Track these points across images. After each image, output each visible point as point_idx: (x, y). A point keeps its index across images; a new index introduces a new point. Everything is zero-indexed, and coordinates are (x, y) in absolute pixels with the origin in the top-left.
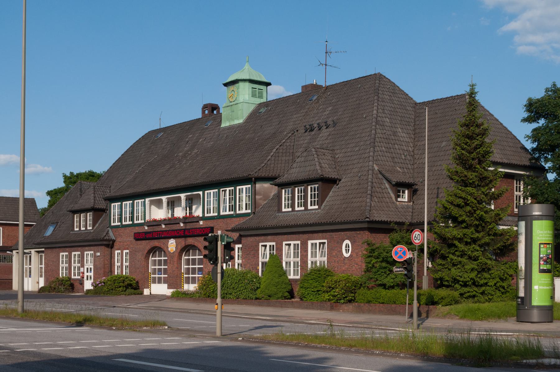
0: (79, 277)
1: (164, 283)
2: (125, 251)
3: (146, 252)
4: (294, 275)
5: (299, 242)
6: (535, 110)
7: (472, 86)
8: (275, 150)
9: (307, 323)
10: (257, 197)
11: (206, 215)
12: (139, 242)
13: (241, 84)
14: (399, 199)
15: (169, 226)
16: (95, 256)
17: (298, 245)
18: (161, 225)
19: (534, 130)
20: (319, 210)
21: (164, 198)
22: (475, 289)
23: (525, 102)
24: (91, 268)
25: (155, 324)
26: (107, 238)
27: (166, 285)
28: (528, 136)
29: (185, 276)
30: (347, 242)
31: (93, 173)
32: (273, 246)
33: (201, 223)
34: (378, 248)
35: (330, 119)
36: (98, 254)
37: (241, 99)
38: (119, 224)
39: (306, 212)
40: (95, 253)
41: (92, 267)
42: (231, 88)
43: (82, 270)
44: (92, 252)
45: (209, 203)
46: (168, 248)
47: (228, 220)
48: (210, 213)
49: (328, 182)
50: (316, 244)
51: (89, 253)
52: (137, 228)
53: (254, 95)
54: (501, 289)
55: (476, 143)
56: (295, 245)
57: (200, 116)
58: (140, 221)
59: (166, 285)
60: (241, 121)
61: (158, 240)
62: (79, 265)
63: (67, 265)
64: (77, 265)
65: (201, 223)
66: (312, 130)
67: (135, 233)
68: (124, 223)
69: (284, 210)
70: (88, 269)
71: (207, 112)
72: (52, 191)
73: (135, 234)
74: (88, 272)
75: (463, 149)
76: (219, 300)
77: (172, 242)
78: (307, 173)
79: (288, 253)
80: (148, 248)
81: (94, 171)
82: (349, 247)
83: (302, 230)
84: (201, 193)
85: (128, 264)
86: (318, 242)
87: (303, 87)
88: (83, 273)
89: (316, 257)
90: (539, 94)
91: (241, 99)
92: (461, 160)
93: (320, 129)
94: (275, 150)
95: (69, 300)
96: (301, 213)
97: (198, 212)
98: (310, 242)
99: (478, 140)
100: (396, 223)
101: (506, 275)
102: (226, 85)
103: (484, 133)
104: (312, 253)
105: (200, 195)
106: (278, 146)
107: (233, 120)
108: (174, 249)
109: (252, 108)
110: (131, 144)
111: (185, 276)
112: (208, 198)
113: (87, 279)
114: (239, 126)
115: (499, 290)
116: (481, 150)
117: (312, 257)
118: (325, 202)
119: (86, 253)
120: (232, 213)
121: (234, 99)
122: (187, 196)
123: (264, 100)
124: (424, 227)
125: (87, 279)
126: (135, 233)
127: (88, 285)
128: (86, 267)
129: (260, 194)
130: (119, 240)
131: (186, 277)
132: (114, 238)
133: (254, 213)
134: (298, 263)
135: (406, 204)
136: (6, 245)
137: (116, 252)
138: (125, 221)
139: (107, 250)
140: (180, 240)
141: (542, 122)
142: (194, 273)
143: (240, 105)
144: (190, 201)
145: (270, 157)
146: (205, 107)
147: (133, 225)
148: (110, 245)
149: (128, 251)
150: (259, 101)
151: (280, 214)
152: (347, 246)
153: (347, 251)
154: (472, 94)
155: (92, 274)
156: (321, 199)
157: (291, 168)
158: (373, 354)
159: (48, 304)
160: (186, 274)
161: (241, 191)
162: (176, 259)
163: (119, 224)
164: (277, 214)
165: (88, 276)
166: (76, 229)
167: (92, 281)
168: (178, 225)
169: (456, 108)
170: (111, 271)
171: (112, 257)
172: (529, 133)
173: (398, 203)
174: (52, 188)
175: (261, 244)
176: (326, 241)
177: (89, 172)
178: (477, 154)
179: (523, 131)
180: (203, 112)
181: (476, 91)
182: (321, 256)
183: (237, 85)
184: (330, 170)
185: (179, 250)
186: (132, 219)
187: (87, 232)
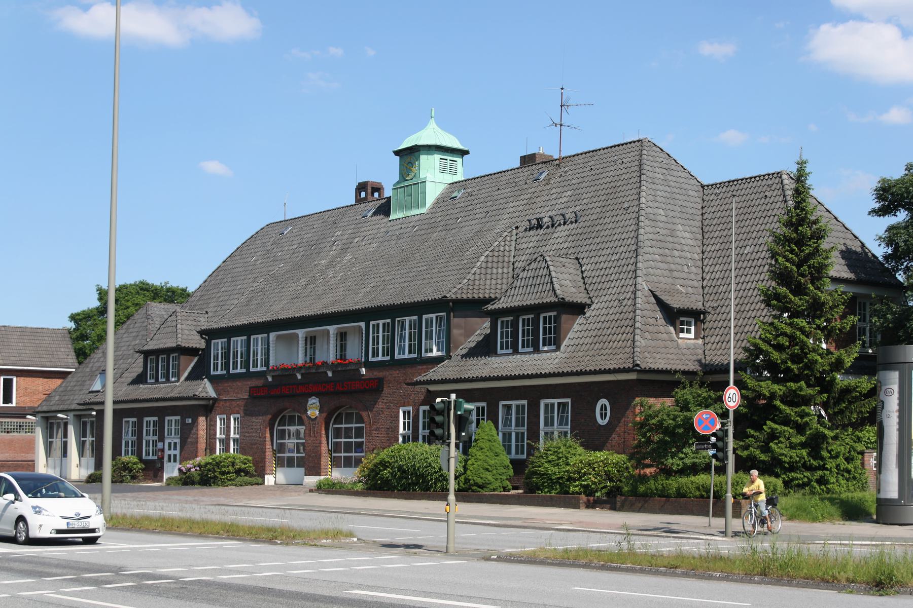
1: (298, 466)
5: (525, 402)
6: (890, 197)
7: (802, 164)
9: (557, 530)
11: (371, 359)
14: (681, 335)
17: (523, 406)
19: (890, 229)
22: (807, 474)
23: (874, 184)
24: (175, 444)
25: (336, 534)
27: (302, 470)
28: (880, 238)
29: (363, 440)
30: (604, 401)
31: (148, 284)
32: (483, 408)
34: (659, 412)
35: (571, 210)
38: (224, 372)
40: (183, 419)
41: (178, 441)
43: (160, 445)
44: (178, 418)
45: (376, 340)
48: (378, 356)
50: (553, 405)
51: (173, 418)
53: (443, 170)
54: (846, 475)
55: (807, 251)
56: (518, 406)
58: (259, 369)
59: (302, 470)
62: (156, 438)
63: (135, 438)
64: (152, 438)
67: (250, 388)
68: (232, 371)
70: (170, 444)
72: (78, 314)
74: (170, 449)
75: (787, 260)
76: (452, 497)
77: (314, 401)
79: (507, 419)
81: (150, 281)
82: (606, 410)
84: (363, 324)
86: (556, 401)
88: (163, 450)
89: (552, 425)
90: (896, 173)
92: (782, 277)
95: (143, 494)
97: (354, 352)
98: (543, 403)
99: (810, 246)
100: (684, 373)
101: (852, 453)
103: (819, 235)
104: (546, 418)
111: (363, 440)
115: (843, 476)
116: (778, 249)
117: (546, 425)
119: (167, 418)
120: (415, 356)
123: (459, 177)
124: (729, 377)
125: (169, 460)
126: (250, 388)
128: (167, 442)
134: (523, 434)
135: (692, 341)
136: (21, 404)
138: (235, 367)
141: (902, 216)
146: (362, 187)
147: (248, 375)
152: (603, 408)
153: (603, 416)
154: (800, 178)
158: (710, 578)
159: (151, 504)
161: (429, 323)
163: (224, 372)
165: (169, 456)
169: (767, 193)
172: (882, 232)
173: (680, 341)
174: (77, 309)
176: (569, 400)
177: (141, 282)
178: (809, 267)
179: (872, 233)
181: (807, 170)
184: (574, 290)
185: (324, 415)
186: (246, 364)
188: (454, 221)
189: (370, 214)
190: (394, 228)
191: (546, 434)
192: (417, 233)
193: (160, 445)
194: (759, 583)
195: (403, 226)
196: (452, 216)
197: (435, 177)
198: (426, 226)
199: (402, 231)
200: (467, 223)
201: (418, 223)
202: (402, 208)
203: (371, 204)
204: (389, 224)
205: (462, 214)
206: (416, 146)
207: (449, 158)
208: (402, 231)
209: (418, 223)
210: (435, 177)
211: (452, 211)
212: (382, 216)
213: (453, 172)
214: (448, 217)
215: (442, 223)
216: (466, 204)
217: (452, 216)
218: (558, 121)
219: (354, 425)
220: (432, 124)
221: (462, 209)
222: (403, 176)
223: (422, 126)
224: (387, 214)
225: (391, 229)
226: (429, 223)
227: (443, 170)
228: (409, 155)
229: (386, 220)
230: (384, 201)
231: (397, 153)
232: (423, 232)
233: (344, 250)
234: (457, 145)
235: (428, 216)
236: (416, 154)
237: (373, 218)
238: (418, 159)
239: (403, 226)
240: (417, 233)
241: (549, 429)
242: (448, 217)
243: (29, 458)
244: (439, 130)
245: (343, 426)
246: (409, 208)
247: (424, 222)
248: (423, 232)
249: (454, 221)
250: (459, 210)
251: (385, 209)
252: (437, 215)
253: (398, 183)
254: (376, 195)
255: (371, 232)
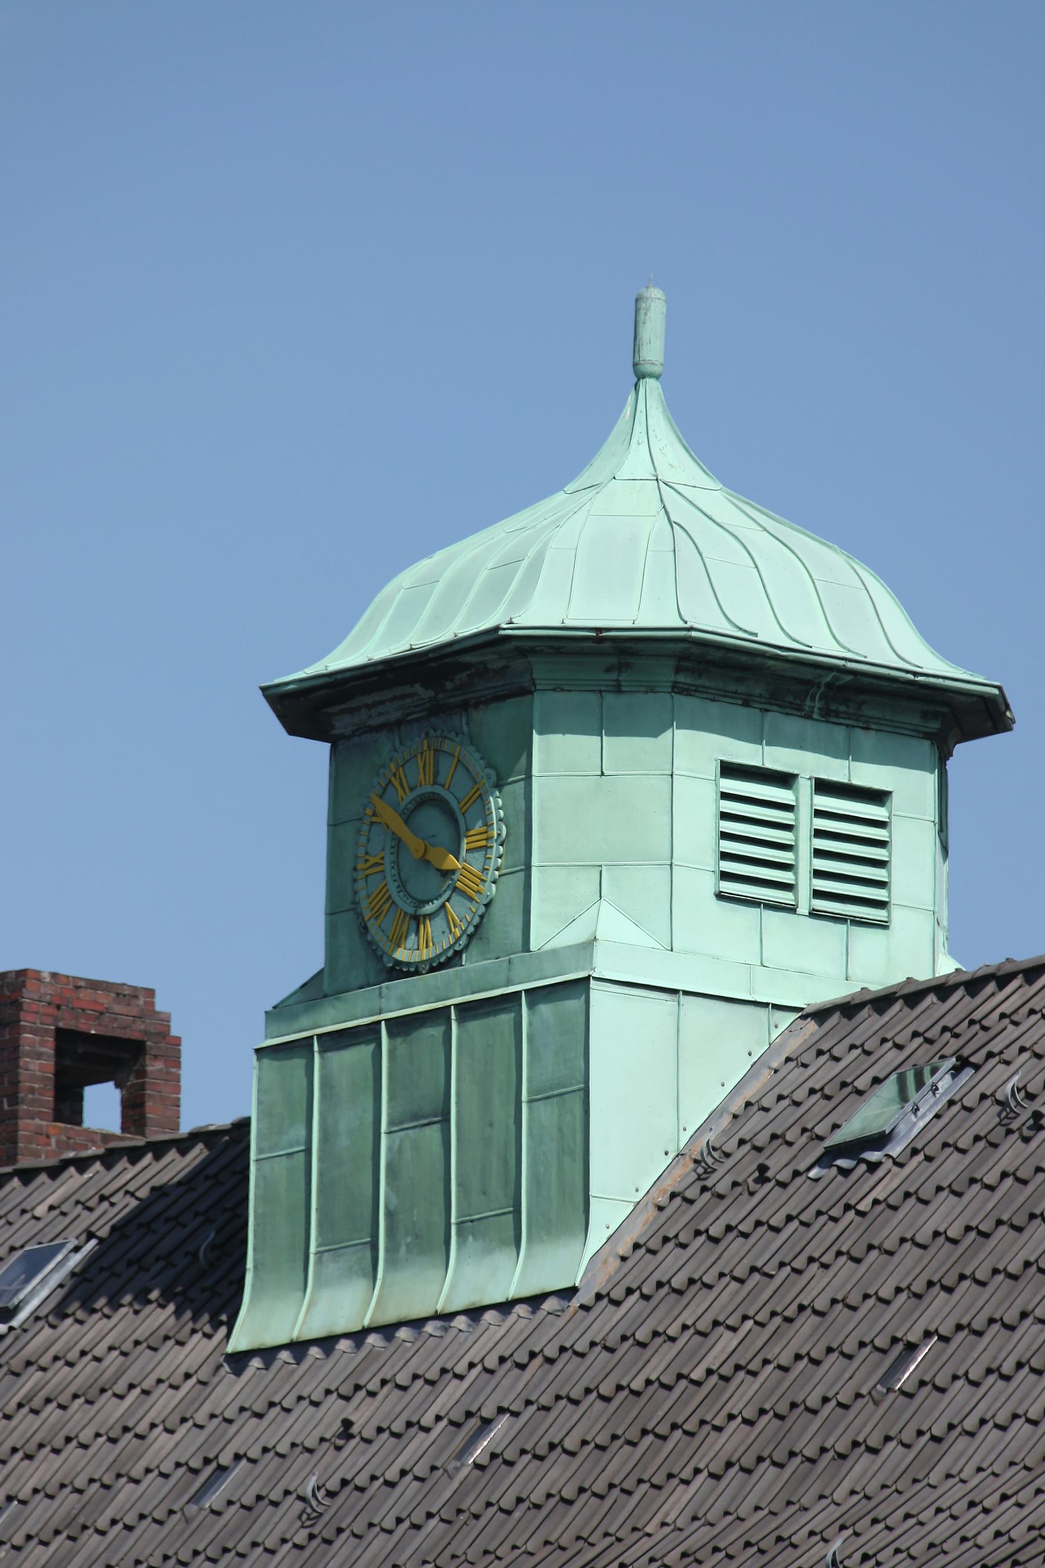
53: (748, 878)
123: (910, 948)
188: (866, 1373)
189: (38, 1293)
190: (279, 1431)
192: (506, 1487)
194: (81, 979)
195: (364, 1414)
196: (846, 1328)
197: (680, 961)
198: (592, 1421)
199: (353, 1461)
200: (996, 1399)
201: (510, 1388)
202: (359, 1240)
203: (50, 1193)
204: (229, 1392)
205: (940, 1312)
206: (492, 641)
207: (809, 764)
208: (353, 1461)
209: (510, 1388)
210: (680, 961)
211: (843, 1277)
212: (159, 1317)
213: (855, 900)
214: (804, 1334)
215: (744, 1395)
216: (978, 1206)
217: (846, 1328)
220: (650, 450)
221: (940, 1262)
222: (365, 931)
223: (559, 453)
224: (212, 1290)
225: (247, 1436)
226: (618, 1377)
227: (748, 878)
228: (424, 742)
229: (199, 1349)
230: (175, 1167)
231: (304, 708)
232: (557, 1475)
234: (887, 638)
235: (607, 1322)
236: (494, 720)
237: (69, 1333)
238: (511, 765)
239: (364, 1414)
240: (506, 1487)
242: (804, 1334)
244: (716, 499)
246: (427, 1241)
247: (573, 1376)
248: (557, 1475)
249: (866, 1373)
250: (906, 1269)
251: (186, 1243)
252: (697, 1309)
253: (314, 992)
254: (102, 1106)
255: (45, 1469)
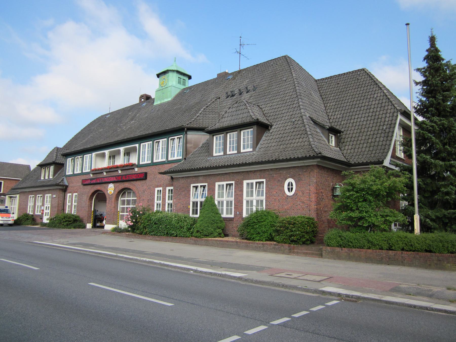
0: (40, 214)
2: (74, 194)
3: (90, 194)
4: (227, 213)
8: (202, 109)
10: (189, 145)
12: (86, 187)
13: (170, 74)
15: (109, 173)
16: (52, 198)
18: (103, 173)
20: (254, 152)
21: (107, 152)
26: (62, 184)
29: (120, 214)
30: (290, 180)
33: (136, 169)
36: (55, 196)
37: (170, 84)
39: (239, 155)
41: (50, 206)
42: (162, 77)
43: (43, 207)
44: (50, 195)
46: (108, 191)
47: (160, 167)
49: (262, 127)
52: (84, 176)
53: (179, 82)
57: (138, 102)
60: (170, 99)
61: (100, 185)
65: (136, 169)
66: (233, 96)
69: (214, 155)
71: (143, 100)
73: (83, 181)
78: (240, 120)
80: (92, 191)
83: (236, 170)
85: (76, 204)
87: (218, 75)
88: (43, 210)
89: (252, 196)
91: (170, 84)
93: (240, 94)
94: (202, 109)
95: (30, 231)
96: (234, 156)
97: (134, 160)
98: (245, 182)
102: (158, 76)
105: (136, 147)
106: (205, 107)
107: (164, 99)
108: (113, 192)
109: (178, 91)
110: (89, 123)
111: (120, 214)
112: (143, 155)
113: (46, 215)
114: (168, 103)
117: (219, 197)
118: (259, 145)
121: (165, 85)
122: (126, 150)
125: (46, 215)
127: (45, 220)
128: (45, 206)
129: (191, 143)
130: (71, 185)
131: (121, 215)
132: (67, 184)
133: (185, 159)
134: (231, 202)
137: (68, 195)
139: (61, 194)
140: (117, 184)
142: (128, 204)
143: (169, 88)
144: (128, 153)
145: (198, 114)
146: (142, 97)
148: (65, 189)
149: (76, 194)
150: (183, 87)
151: (212, 158)
152: (290, 184)
153: (290, 190)
155: (49, 211)
156: (257, 140)
157: (222, 118)
160: (122, 212)
162: (113, 199)
164: (209, 158)
165: (46, 213)
166: (42, 178)
167: (49, 216)
168: (117, 172)
170: (64, 209)
171: (65, 199)
175: (192, 185)
180: (140, 100)
182: (228, 197)
183: (167, 75)
185: (116, 193)
187: (49, 180)
191: (247, 202)
193: (43, 207)
218: (238, 50)
219: (131, 199)
233: (132, 120)
241: (250, 198)
243: (393, 159)
245: (126, 199)
